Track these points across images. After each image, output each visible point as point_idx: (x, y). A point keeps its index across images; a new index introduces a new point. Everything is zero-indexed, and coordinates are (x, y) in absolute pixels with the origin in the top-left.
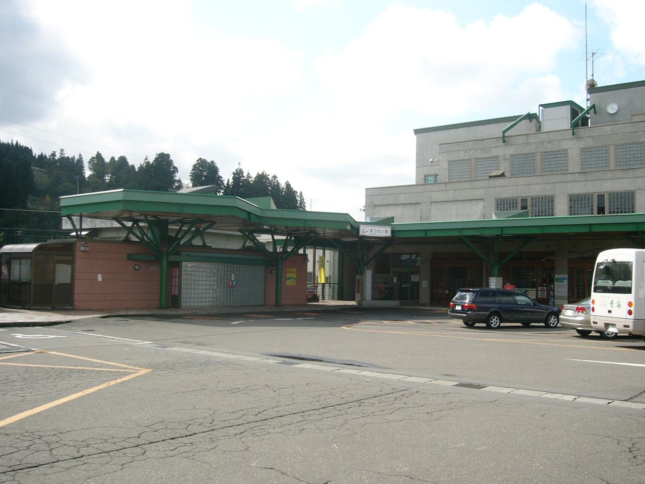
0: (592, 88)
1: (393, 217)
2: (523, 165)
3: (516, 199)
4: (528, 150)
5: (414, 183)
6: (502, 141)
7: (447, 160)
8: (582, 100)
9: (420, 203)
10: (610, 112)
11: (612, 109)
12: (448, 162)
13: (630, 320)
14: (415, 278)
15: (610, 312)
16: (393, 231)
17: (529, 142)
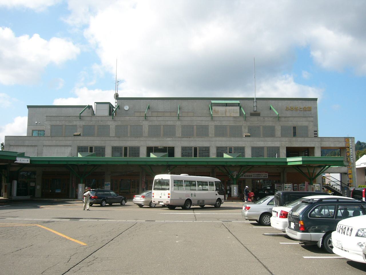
0: (117, 96)
1: (24, 153)
2: (88, 131)
3: (87, 147)
4: (91, 123)
5: (26, 135)
6: (79, 118)
7: (50, 125)
8: (114, 102)
9: (37, 146)
10: (126, 110)
11: (126, 108)
12: (50, 125)
13: (169, 200)
14: (32, 184)
15: (161, 197)
16: (31, 161)
17: (92, 120)
